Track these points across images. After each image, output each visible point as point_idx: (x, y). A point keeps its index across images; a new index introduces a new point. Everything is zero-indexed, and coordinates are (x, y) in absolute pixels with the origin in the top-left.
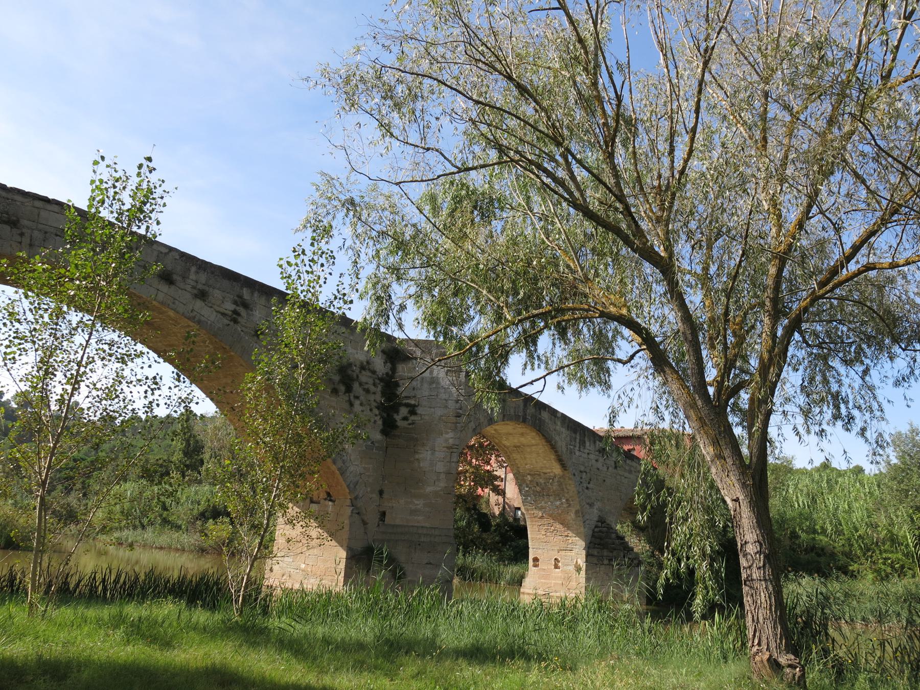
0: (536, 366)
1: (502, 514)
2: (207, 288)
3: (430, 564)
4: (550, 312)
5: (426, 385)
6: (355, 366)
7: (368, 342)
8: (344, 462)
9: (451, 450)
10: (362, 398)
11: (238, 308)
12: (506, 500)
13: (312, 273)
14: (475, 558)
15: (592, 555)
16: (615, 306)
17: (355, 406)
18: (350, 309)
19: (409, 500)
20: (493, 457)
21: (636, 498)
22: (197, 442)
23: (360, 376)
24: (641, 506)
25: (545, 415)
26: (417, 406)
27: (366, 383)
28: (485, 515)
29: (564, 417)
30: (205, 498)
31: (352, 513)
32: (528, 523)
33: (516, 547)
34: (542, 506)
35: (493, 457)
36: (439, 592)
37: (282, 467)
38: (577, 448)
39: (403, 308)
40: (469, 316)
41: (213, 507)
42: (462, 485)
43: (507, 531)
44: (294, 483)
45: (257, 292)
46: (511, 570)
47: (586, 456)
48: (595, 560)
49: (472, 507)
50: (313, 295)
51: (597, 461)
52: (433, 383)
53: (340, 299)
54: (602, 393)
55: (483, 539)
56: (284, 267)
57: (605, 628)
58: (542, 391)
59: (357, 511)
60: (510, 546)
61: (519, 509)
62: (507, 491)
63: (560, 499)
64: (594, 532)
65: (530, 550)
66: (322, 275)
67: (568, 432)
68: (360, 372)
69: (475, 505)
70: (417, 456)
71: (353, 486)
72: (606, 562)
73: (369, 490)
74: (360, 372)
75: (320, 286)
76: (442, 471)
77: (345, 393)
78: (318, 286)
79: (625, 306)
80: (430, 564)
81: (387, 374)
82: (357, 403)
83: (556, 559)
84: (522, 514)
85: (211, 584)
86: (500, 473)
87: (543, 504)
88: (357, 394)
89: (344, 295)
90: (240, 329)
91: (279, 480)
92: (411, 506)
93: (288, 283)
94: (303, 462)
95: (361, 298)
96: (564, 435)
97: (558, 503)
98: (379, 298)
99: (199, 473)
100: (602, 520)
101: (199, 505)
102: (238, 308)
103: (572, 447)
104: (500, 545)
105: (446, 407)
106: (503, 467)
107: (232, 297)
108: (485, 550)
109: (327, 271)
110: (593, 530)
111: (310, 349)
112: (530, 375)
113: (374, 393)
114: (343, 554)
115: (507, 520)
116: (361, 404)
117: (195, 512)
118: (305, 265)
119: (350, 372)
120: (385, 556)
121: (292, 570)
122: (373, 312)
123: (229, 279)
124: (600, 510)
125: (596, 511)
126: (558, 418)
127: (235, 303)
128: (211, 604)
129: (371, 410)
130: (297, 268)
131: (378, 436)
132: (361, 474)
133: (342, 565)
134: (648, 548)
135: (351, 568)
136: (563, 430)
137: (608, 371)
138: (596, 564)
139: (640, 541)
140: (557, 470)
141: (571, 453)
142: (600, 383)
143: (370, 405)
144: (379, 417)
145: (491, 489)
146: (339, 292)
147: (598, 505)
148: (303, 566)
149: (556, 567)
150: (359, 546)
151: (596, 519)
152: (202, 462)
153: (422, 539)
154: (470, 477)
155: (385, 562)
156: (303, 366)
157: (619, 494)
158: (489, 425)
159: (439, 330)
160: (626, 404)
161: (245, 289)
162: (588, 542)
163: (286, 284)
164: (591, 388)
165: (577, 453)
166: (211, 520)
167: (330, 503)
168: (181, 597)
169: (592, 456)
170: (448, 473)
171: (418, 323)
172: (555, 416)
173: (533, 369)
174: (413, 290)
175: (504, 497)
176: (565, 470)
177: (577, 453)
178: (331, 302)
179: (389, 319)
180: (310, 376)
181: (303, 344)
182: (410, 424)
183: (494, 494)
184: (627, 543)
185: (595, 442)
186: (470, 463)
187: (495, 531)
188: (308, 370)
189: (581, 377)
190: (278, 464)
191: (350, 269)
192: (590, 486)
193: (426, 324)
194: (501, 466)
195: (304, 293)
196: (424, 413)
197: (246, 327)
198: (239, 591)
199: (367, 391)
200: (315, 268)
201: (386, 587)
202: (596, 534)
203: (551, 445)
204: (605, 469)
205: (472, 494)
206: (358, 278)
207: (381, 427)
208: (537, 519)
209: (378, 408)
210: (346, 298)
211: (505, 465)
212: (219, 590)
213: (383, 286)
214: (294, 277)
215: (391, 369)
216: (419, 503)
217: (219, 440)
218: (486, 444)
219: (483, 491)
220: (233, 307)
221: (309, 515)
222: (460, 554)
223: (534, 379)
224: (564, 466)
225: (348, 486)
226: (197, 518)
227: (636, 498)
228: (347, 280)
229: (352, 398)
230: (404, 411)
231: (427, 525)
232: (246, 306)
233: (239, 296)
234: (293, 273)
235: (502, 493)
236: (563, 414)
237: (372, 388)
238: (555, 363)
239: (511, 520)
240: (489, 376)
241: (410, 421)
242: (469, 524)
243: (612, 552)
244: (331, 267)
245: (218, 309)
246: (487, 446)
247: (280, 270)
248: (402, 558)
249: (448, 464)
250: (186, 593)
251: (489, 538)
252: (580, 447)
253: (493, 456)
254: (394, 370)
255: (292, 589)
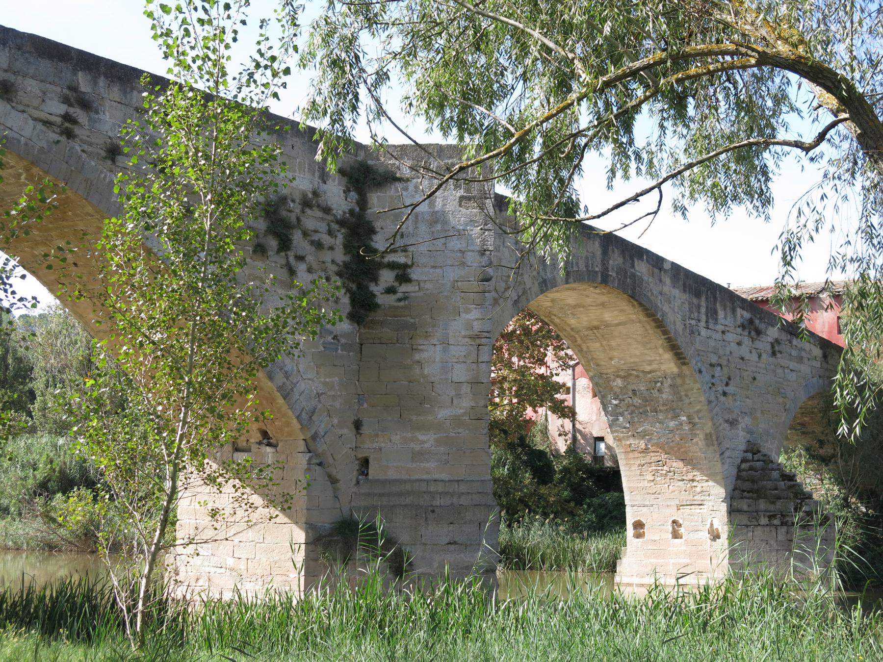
0: (632, 171)
1: (572, 450)
2: (11, 77)
3: (455, 543)
4: (663, 61)
5: (423, 228)
6: (293, 201)
7: (321, 145)
8: (287, 375)
9: (478, 341)
10: (309, 258)
11: (71, 110)
12: (578, 426)
13: (210, 22)
14: (529, 530)
15: (739, 511)
16: (786, 40)
17: (299, 274)
18: (284, 85)
19: (409, 435)
20: (550, 353)
21: (838, 394)
22: (19, 360)
23: (302, 218)
24: (846, 409)
25: (642, 268)
26: (410, 267)
27: (316, 231)
28: (542, 454)
29: (677, 269)
30: (44, 458)
31: (309, 464)
32: (622, 464)
33: (600, 506)
34: (644, 431)
35: (550, 353)
36: (481, 589)
37: (190, 384)
38: (703, 324)
39: (382, 77)
40: (503, 87)
41: (60, 472)
42: (496, 405)
43: (583, 480)
44: (212, 410)
45: (102, 78)
46: (598, 546)
47: (718, 336)
48: (744, 519)
49: (517, 441)
50: (215, 65)
51: (739, 344)
52: (436, 222)
53: (266, 67)
54: (755, 214)
55: (541, 497)
56: (156, 16)
57: (787, 632)
58: (656, 213)
59: (318, 461)
60: (589, 506)
61: (601, 439)
62: (577, 410)
63: (676, 417)
64: (739, 470)
65: (628, 510)
66: (228, 25)
67: (685, 296)
68: (303, 212)
69: (522, 439)
70: (417, 357)
71: (306, 418)
72: (764, 521)
73: (336, 421)
74: (303, 212)
75: (227, 47)
76: (462, 380)
77: (279, 251)
78: (222, 46)
79: (802, 42)
80: (455, 543)
81: (351, 212)
82: (301, 268)
83: (674, 522)
84: (608, 447)
85: (79, 600)
86: (564, 377)
87: (647, 426)
88: (300, 253)
89: (273, 59)
90: (78, 149)
91: (186, 407)
92: (412, 445)
93: (168, 46)
94: (225, 371)
95: (303, 64)
96: (678, 302)
97: (672, 424)
98: (336, 63)
99: (30, 414)
100: (753, 449)
101: (35, 470)
102: (71, 110)
103: (693, 322)
104: (572, 504)
105: (463, 264)
106: (569, 367)
107: (59, 89)
108: (545, 515)
109: (237, 16)
110: (739, 467)
111: (219, 165)
112: (624, 189)
113: (331, 248)
114: (300, 536)
115: (581, 459)
116: (310, 270)
117: (30, 482)
118: (196, 9)
119: (284, 213)
120: (379, 532)
121: (212, 570)
122: (326, 87)
123: (51, 57)
124: (750, 432)
125: (742, 433)
126: (666, 271)
127: (66, 100)
128: (83, 634)
129: (328, 279)
130: (181, 17)
131: (345, 326)
132: (319, 395)
133: (300, 557)
134: (836, 492)
135: (316, 560)
136: (676, 292)
137: (764, 171)
138: (747, 526)
139: (822, 480)
140: (668, 364)
141: (692, 332)
142: (750, 194)
143: (325, 270)
144: (343, 291)
145: (550, 408)
146: (262, 55)
147: (745, 422)
148: (231, 562)
149: (676, 535)
150: (326, 521)
151: (743, 447)
152: (32, 395)
153: (437, 502)
154: (510, 389)
155: (381, 543)
156: (209, 197)
157: (781, 400)
158: (542, 292)
159: (448, 115)
160: (811, 225)
161: (80, 74)
162: (731, 487)
163: (164, 49)
164: (734, 206)
165: (704, 332)
166: (59, 495)
167: (269, 449)
168: (29, 625)
169: (730, 337)
170: (475, 383)
171: (411, 104)
172: (660, 269)
173: (626, 177)
174: (397, 44)
175: (573, 421)
176: (684, 364)
177: (704, 332)
178: (251, 75)
179: (357, 100)
180: (224, 215)
181: (207, 157)
182: (400, 300)
183: (555, 416)
184: (800, 485)
185: (734, 311)
186: (509, 365)
187: (561, 481)
188: (218, 203)
189: (715, 185)
190: (182, 378)
191: (279, 10)
192: (730, 389)
193: (424, 106)
194: (565, 366)
195: (199, 62)
196: (424, 278)
197: (90, 144)
198: (135, 606)
199: (318, 245)
200: (213, 13)
201: (386, 585)
202: (744, 474)
203: (656, 321)
204: (754, 357)
205: (515, 418)
206: (295, 25)
207: (348, 309)
208: (636, 455)
209: (339, 274)
210: (275, 65)
211: (572, 363)
212: (94, 608)
213: (343, 39)
214: (177, 32)
215: (358, 203)
216: (428, 439)
217: (59, 354)
218: (535, 328)
219: (536, 412)
220: (62, 109)
221: (240, 473)
222: (502, 526)
223: (639, 191)
224: (679, 356)
225: (298, 418)
226: (35, 492)
227: (838, 394)
228: (274, 31)
229: (292, 260)
230: (387, 277)
231: (444, 476)
232: (85, 104)
233: (70, 88)
234: (175, 27)
235: (568, 413)
236: (673, 264)
237: (327, 240)
238: (665, 162)
239: (588, 459)
240: (547, 196)
241: (399, 295)
242: (513, 471)
243: (773, 503)
244: (242, 10)
245: (36, 114)
246: (537, 331)
247: (150, 22)
248: (403, 537)
249: (474, 366)
250: (37, 617)
251: (552, 494)
252: (707, 322)
253: (550, 348)
254: (363, 203)
255: (220, 600)
